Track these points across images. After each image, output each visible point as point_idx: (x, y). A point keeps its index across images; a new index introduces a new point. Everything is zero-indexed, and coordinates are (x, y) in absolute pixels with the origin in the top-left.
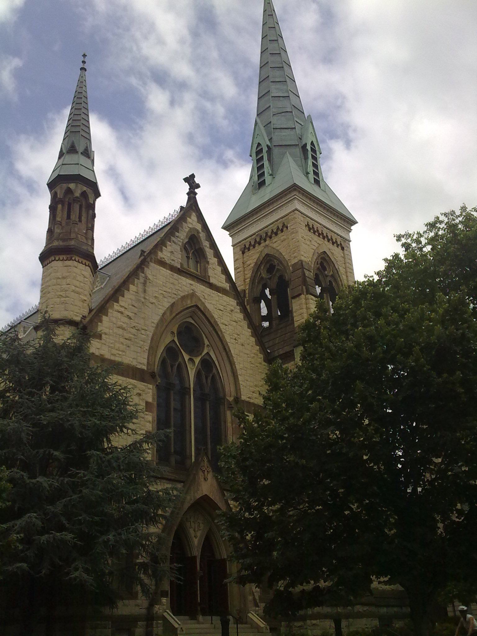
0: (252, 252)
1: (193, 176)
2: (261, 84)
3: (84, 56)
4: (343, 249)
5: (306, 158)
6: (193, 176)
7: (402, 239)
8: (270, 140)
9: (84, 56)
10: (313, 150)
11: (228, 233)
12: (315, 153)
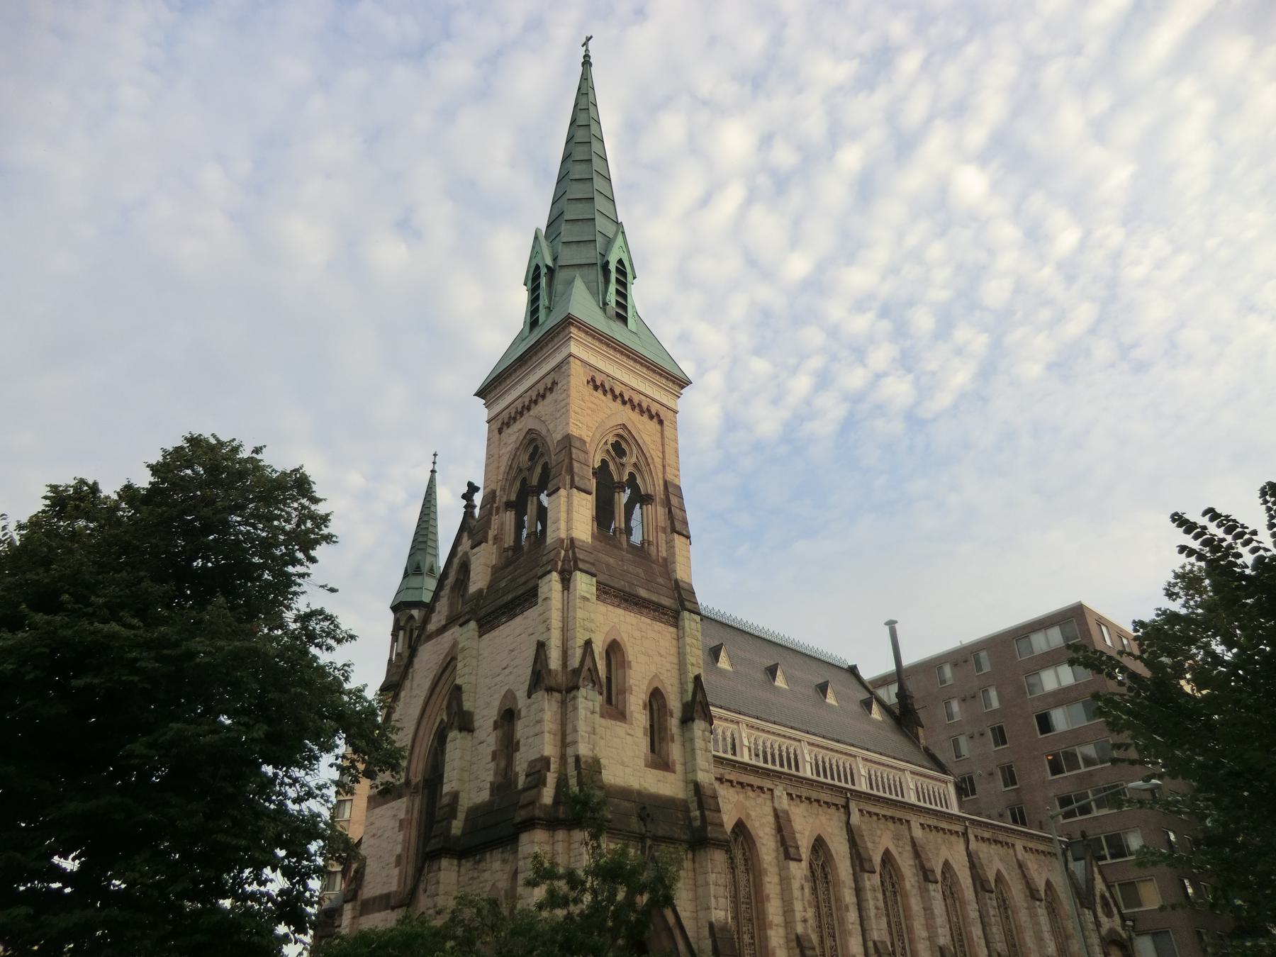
0: (510, 431)
2: (847, 676)
4: (661, 422)
5: (607, 282)
7: (1081, 653)
8: (555, 259)
10: (621, 271)
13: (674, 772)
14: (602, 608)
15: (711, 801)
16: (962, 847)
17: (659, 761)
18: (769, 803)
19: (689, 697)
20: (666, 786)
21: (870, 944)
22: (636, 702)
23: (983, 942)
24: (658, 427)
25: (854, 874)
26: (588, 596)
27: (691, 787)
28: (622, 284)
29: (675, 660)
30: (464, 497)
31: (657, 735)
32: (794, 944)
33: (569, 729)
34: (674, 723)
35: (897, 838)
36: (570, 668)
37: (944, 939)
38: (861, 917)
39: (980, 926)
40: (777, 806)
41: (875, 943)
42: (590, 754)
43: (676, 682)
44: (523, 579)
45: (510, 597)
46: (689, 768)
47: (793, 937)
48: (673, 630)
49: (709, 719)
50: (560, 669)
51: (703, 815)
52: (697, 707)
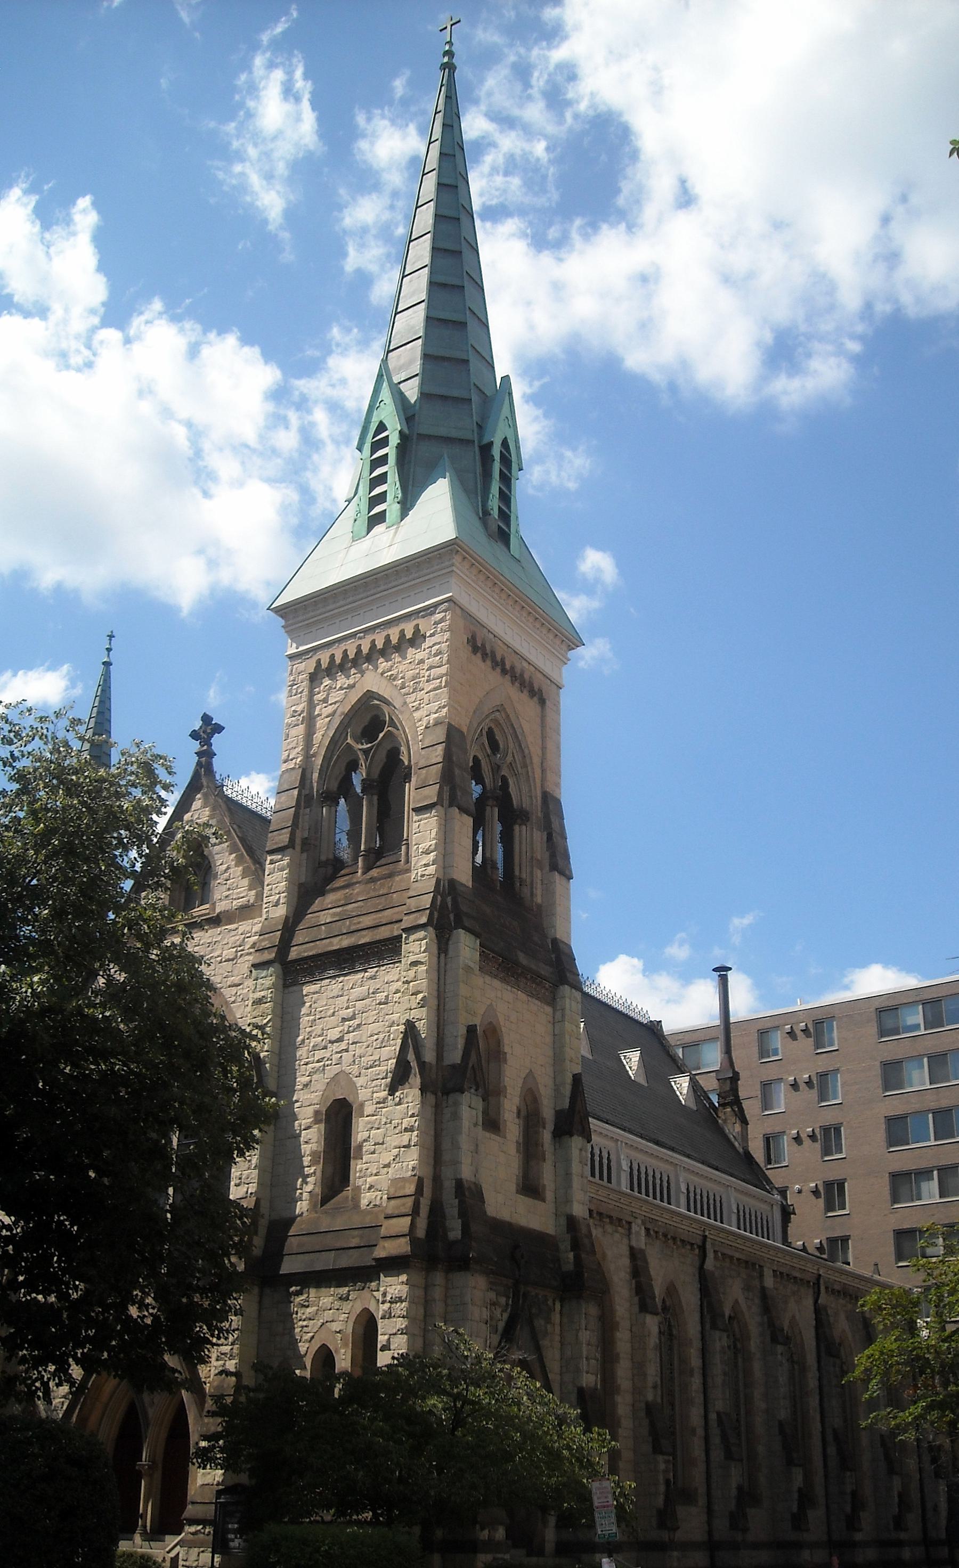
1: (219, 729)
3: (111, 637)
6: (219, 729)
9: (111, 637)
10: (506, 460)
11: (282, 622)
12: (509, 468)
13: (544, 1200)
14: (480, 980)
15: (586, 1241)
16: (809, 1302)
17: (530, 1188)
18: (625, 1241)
19: (566, 1104)
20: (535, 1217)
21: (713, 1416)
22: (510, 1106)
23: (818, 1417)
24: (539, 709)
25: (703, 1333)
26: (472, 965)
27: (563, 1221)
28: (506, 480)
29: (550, 1053)
30: (195, 735)
31: (530, 1150)
32: (643, 1414)
33: (446, 1144)
34: (547, 1136)
35: (747, 1288)
36: (447, 1062)
37: (720, 1403)
38: (705, 1384)
39: (817, 1397)
40: (634, 1243)
41: (718, 1414)
42: (473, 1179)
43: (550, 1083)
44: (367, 921)
45: (346, 942)
46: (564, 1199)
47: (643, 1405)
48: (549, 1010)
49: (586, 1135)
50: (434, 1062)
51: (577, 1258)
52: (572, 1122)
